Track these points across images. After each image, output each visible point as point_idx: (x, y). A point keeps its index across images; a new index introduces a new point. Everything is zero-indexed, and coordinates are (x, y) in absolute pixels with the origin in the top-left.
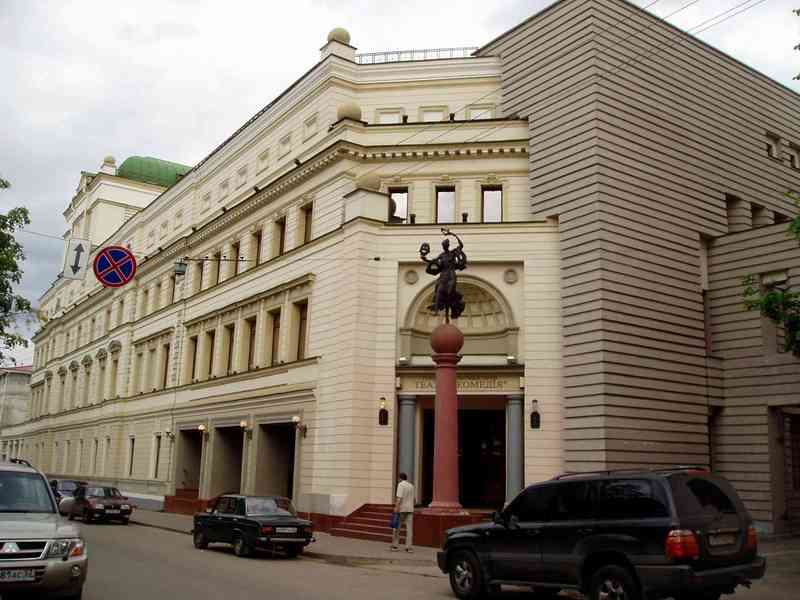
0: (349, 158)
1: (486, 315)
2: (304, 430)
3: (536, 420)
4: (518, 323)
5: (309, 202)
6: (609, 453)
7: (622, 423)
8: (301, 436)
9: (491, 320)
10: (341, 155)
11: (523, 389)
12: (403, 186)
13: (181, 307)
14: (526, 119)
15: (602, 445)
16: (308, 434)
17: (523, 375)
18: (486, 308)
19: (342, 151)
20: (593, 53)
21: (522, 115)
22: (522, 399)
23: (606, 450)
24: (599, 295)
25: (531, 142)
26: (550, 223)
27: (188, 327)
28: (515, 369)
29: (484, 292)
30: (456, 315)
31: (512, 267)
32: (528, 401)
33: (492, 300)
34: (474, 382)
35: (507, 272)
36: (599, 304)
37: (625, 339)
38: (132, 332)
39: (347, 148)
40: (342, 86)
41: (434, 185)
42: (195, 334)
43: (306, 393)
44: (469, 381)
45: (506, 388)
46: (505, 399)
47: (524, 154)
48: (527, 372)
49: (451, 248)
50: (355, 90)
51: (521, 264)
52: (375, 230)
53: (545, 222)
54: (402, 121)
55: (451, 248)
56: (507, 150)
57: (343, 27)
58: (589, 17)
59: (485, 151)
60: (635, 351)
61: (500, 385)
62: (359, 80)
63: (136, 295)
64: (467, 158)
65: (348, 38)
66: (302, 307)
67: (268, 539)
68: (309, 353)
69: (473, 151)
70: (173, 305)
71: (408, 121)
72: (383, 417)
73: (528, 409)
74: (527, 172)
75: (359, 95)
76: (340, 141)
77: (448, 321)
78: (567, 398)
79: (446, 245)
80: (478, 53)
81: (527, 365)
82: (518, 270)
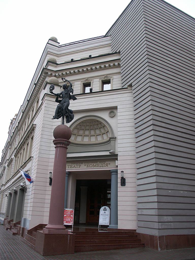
1: (103, 134)
4: (116, 136)
7: (166, 180)
9: (105, 136)
11: (117, 166)
15: (155, 199)
17: (117, 159)
18: (103, 131)
20: (149, 80)
21: (117, 51)
22: (116, 172)
23: (157, 195)
24: (154, 167)
26: (129, 88)
28: (114, 157)
29: (101, 123)
31: (112, 110)
32: (119, 172)
33: (104, 126)
34: (95, 164)
35: (110, 113)
36: (154, 167)
37: (166, 140)
40: (52, 55)
44: (92, 164)
45: (109, 167)
46: (109, 173)
47: (119, 66)
48: (119, 158)
50: (57, 56)
51: (116, 108)
56: (112, 65)
57: (55, 37)
58: (144, 38)
59: (103, 66)
60: (183, 97)
61: (107, 165)
62: (59, 53)
69: (98, 67)
71: (93, 91)
73: (119, 176)
74: (120, 73)
75: (59, 58)
77: (63, 123)
78: (138, 169)
81: (119, 154)
82: (115, 111)
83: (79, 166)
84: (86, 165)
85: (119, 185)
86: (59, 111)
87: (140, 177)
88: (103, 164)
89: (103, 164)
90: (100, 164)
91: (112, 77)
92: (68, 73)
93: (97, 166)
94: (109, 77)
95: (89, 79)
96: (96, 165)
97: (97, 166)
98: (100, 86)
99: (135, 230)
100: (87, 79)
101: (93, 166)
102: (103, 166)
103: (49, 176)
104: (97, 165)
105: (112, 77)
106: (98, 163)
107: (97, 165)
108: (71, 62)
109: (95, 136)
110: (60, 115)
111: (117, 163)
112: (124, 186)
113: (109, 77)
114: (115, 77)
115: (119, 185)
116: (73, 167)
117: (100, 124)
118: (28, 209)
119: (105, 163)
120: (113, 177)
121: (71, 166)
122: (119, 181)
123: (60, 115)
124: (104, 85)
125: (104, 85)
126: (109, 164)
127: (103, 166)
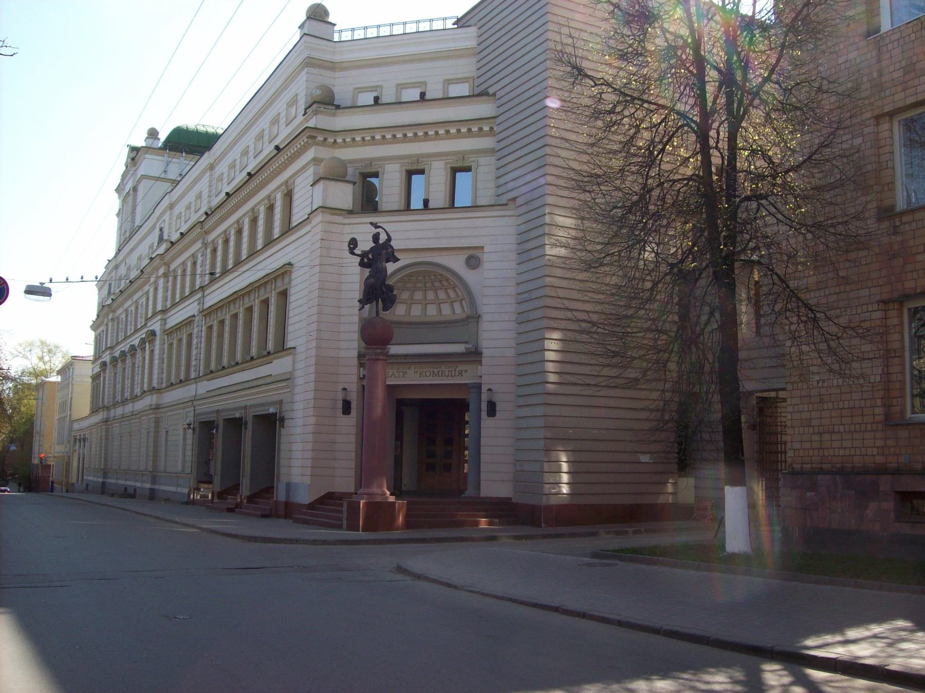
0: (317, 144)
2: (282, 420)
3: (492, 409)
4: (480, 312)
5: (290, 189)
6: (548, 441)
8: (280, 426)
10: (310, 141)
11: (481, 376)
12: (373, 170)
13: (199, 295)
14: (494, 94)
16: (285, 424)
19: (311, 135)
21: (491, 91)
22: (478, 387)
25: (498, 121)
27: (205, 316)
28: (474, 355)
30: (386, 308)
32: (484, 389)
38: (165, 320)
39: (315, 135)
41: (449, 166)
42: (222, 318)
43: (287, 379)
45: (465, 376)
49: (381, 242)
52: (339, 219)
53: (506, 205)
54: (418, 98)
55: (381, 242)
61: (461, 373)
63: (168, 282)
64: (435, 139)
65: (326, 13)
66: (284, 294)
67: (467, 462)
68: (290, 344)
70: (193, 292)
72: (347, 408)
73: (484, 397)
75: (337, 74)
76: (307, 127)
79: (376, 238)
80: (461, 22)
83: (404, 374)
85: (484, 414)
87: (521, 401)
91: (426, 164)
92: (369, 140)
93: (440, 375)
94: (376, 166)
95: (421, 160)
96: (438, 372)
97: (440, 375)
98: (446, 181)
99: (510, 499)
100: (418, 158)
102: (453, 375)
103: (340, 396)
104: (440, 372)
105: (474, 161)
106: (443, 368)
107: (440, 372)
108: (181, 238)
111: (482, 370)
113: (376, 166)
114: (483, 160)
115: (484, 414)
118: (299, 430)
119: (458, 370)
122: (484, 406)
124: (413, 176)
125: (413, 176)
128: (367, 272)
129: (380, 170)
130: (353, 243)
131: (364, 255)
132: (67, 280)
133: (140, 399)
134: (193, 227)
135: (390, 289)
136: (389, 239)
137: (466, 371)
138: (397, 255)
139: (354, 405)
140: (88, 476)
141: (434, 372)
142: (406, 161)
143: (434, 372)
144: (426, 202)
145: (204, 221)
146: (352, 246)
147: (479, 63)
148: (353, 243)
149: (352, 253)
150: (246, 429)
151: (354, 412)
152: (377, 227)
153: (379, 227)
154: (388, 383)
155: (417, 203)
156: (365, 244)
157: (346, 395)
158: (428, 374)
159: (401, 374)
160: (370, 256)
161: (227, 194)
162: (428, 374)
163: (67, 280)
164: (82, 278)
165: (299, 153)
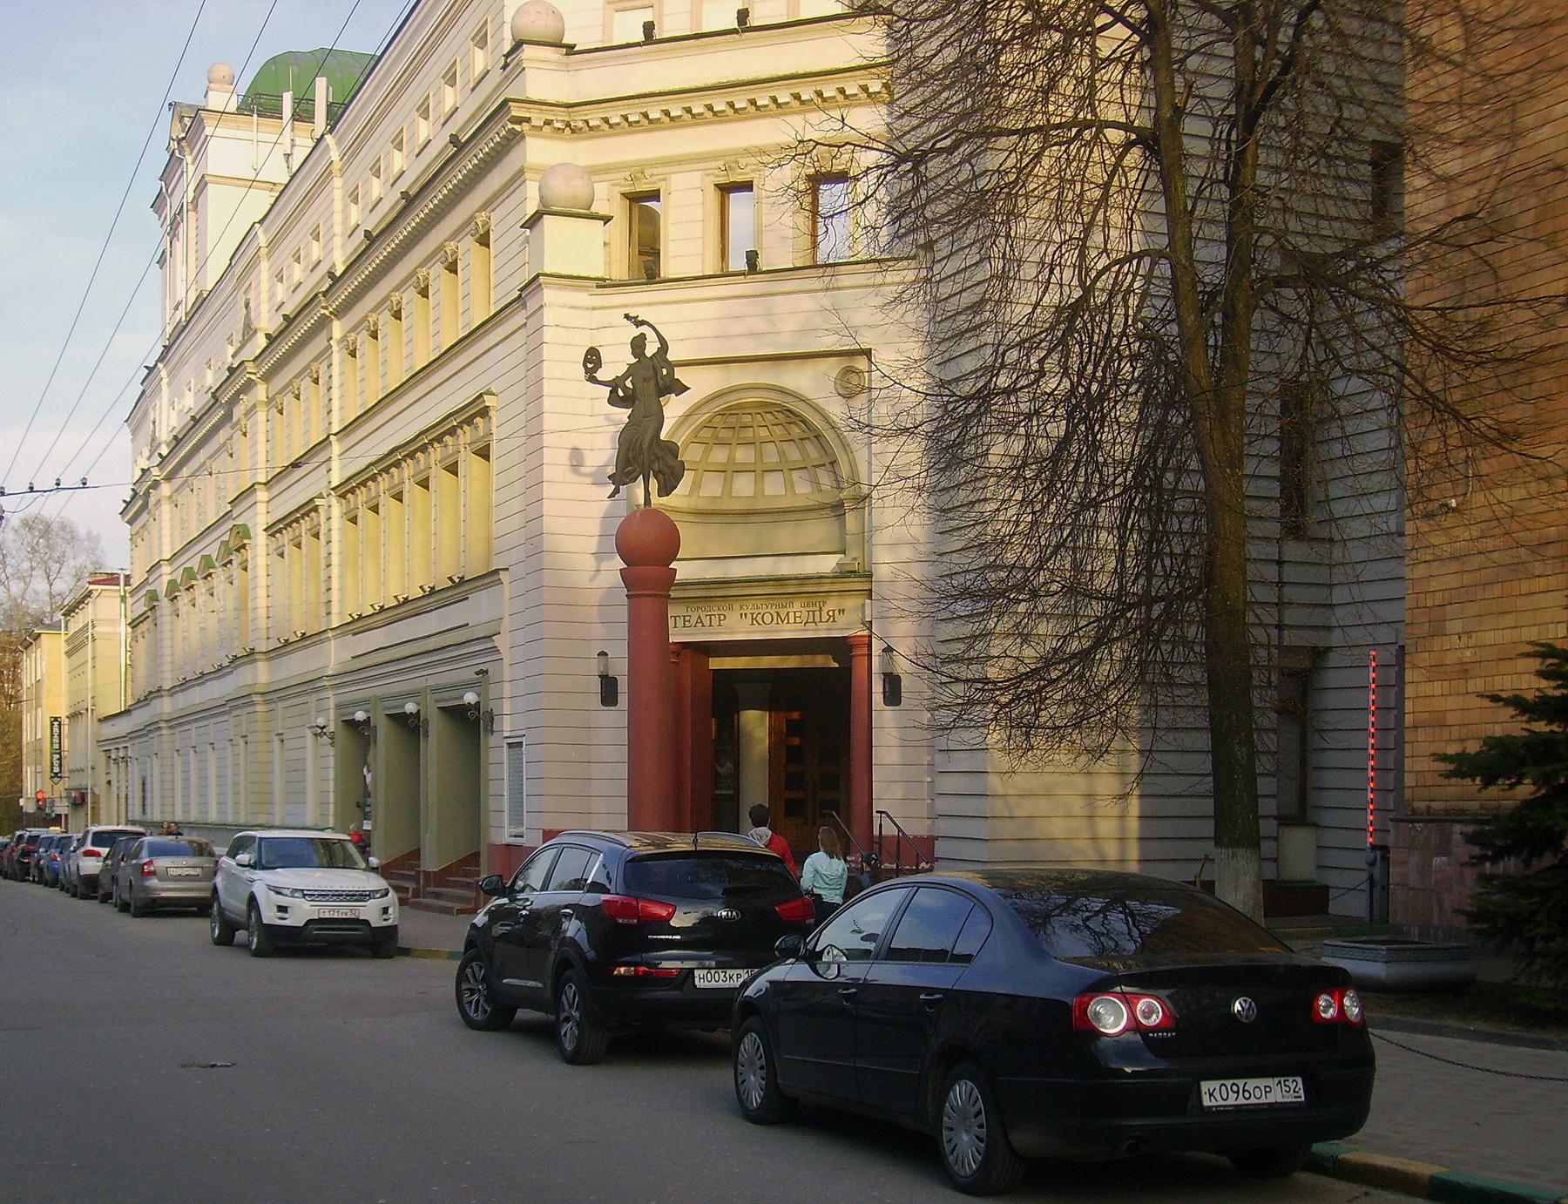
12: (645, 188)
28: (271, 793)
30: (665, 490)
46: (842, 647)
72: (609, 691)
79: (638, 344)
84: (749, 616)
86: (627, 456)
88: (817, 613)
89: (817, 613)
90: (803, 610)
93: (792, 620)
94: (654, 178)
97: (792, 620)
101: (775, 621)
102: (817, 619)
103: (594, 667)
104: (792, 615)
107: (792, 615)
109: (805, 468)
110: (634, 470)
112: (897, 708)
116: (693, 621)
117: (816, 437)
120: (859, 665)
121: (687, 618)
123: (634, 470)
126: (839, 611)
127: (817, 619)
128: (623, 414)
129: (661, 186)
130: (593, 359)
131: (614, 384)
132: (31, 488)
133: (228, 673)
134: (740, 581)
135: (672, 449)
136: (664, 347)
137: (842, 611)
138: (679, 374)
139: (623, 686)
140: (254, 469)
141: (778, 614)
142: (714, 164)
143: (778, 614)
144: (752, 257)
145: (328, 290)
146: (590, 366)
147: (516, 168)
148: (593, 359)
149: (593, 380)
150: (426, 735)
151: (623, 699)
152: (639, 323)
153: (643, 323)
154: (677, 636)
155: (738, 263)
156: (617, 362)
157: (606, 666)
158: (768, 618)
159: (715, 621)
160: (629, 384)
161: (367, 234)
162: (768, 618)
163: (31, 488)
164: (58, 484)
165: (498, 152)
